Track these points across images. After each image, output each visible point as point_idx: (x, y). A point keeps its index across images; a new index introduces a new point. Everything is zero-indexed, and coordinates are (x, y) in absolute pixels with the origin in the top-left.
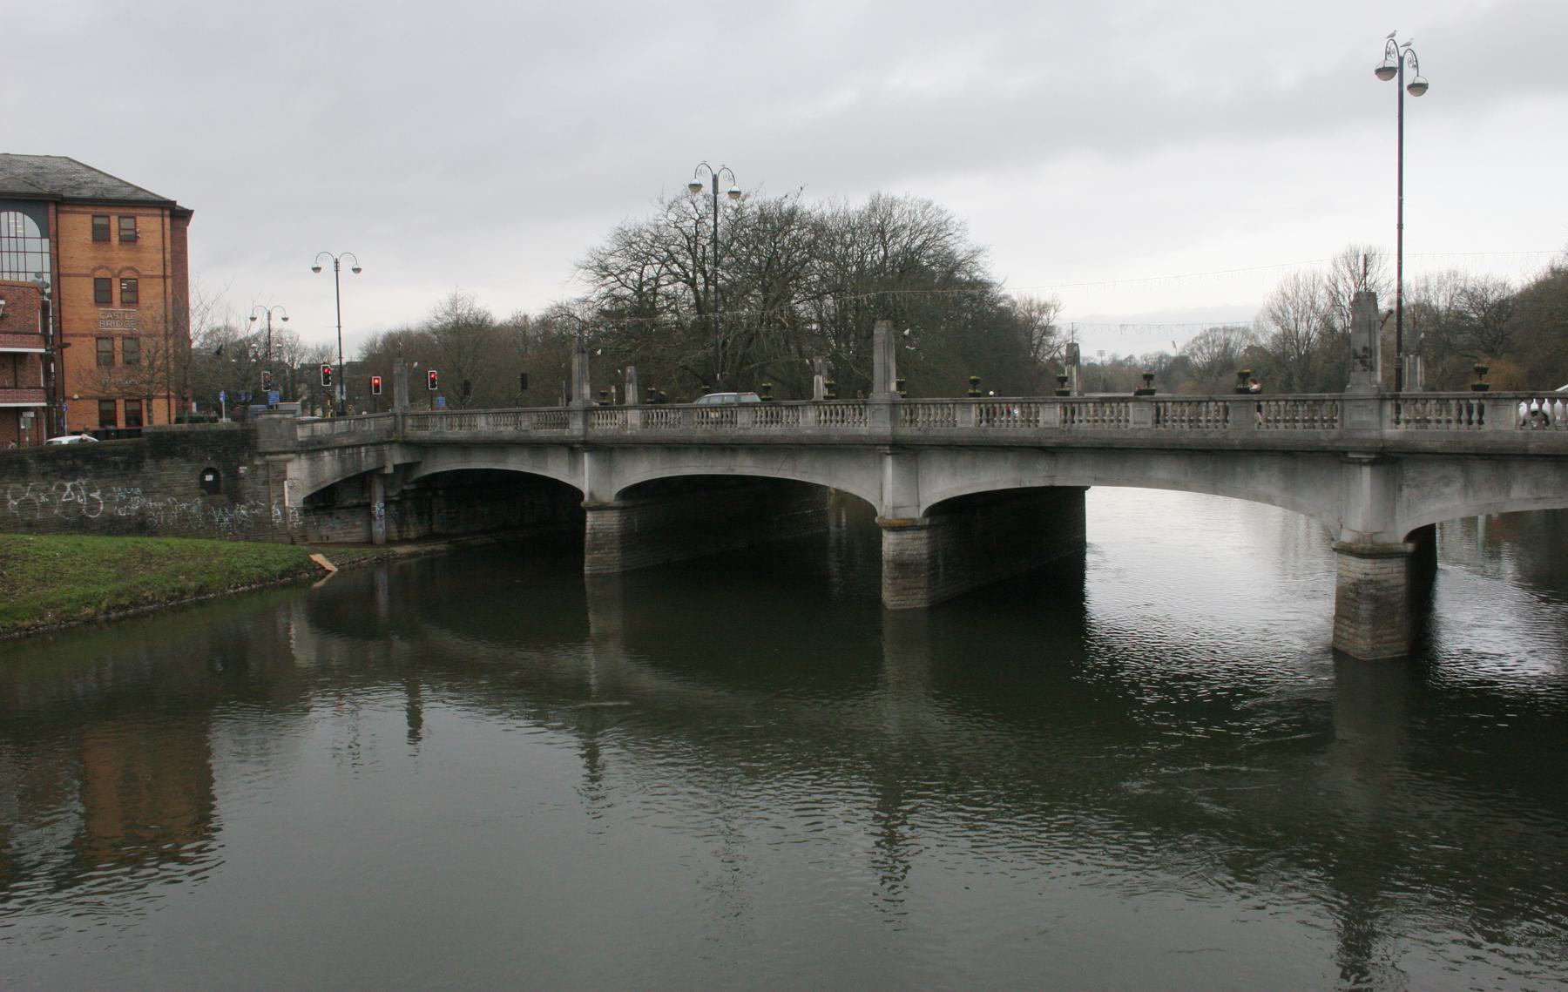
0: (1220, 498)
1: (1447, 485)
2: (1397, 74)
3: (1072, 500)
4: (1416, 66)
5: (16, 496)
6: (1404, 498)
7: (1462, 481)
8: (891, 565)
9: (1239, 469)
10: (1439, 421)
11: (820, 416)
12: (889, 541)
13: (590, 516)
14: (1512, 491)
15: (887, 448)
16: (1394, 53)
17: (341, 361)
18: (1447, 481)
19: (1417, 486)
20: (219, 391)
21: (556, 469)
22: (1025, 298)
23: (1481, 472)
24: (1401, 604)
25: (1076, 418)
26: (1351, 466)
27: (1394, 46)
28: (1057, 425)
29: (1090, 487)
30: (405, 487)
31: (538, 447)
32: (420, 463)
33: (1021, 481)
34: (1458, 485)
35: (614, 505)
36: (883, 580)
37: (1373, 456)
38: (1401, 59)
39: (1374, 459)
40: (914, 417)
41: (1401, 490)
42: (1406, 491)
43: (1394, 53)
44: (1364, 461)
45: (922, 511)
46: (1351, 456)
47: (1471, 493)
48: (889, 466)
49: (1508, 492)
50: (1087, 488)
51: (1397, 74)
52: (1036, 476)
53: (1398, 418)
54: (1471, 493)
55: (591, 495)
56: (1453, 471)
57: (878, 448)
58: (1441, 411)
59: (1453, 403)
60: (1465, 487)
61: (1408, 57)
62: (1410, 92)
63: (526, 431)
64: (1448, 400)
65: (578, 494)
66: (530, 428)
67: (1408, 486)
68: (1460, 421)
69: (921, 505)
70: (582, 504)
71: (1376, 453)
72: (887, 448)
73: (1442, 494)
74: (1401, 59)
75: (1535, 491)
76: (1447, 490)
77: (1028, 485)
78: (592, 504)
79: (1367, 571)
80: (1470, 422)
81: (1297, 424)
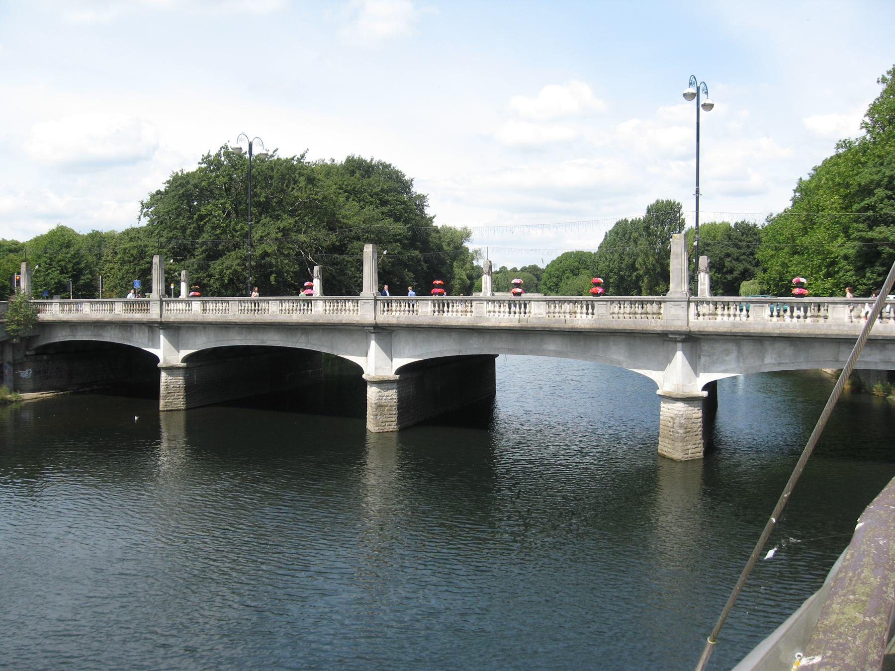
0: (690, 368)
1: (727, 355)
2: (696, 97)
3: (487, 363)
4: (707, 93)
5: (1, 531)
6: (701, 363)
7: (736, 352)
8: (374, 406)
9: (600, 344)
10: (499, 312)
11: (384, 307)
12: (372, 393)
13: (163, 375)
14: (765, 359)
15: (372, 328)
16: (694, 84)
17: (179, 368)
18: (728, 353)
19: (710, 356)
20: (312, 266)
21: (139, 341)
22: (636, 219)
23: (747, 348)
24: (700, 429)
25: (450, 309)
26: (670, 343)
27: (694, 80)
28: (429, 314)
29: (498, 355)
30: (28, 353)
31: (125, 325)
32: (38, 336)
33: (460, 351)
34: (734, 355)
35: (180, 366)
36: (367, 416)
37: (684, 337)
38: (698, 89)
39: (684, 338)
40: (390, 308)
41: (700, 358)
42: (703, 359)
43: (694, 84)
44: (678, 339)
45: (394, 372)
46: (671, 336)
47: (741, 360)
48: (680, 357)
49: (763, 360)
50: (497, 356)
51: (696, 97)
52: (474, 348)
53: (772, 314)
54: (741, 360)
55: (165, 359)
56: (732, 347)
57: (366, 328)
58: (724, 308)
59: (517, 302)
60: (738, 357)
61: (702, 86)
62: (703, 109)
63: (118, 314)
64: (865, 303)
65: (156, 359)
66: (122, 312)
67: (704, 355)
68: (587, 314)
69: (393, 366)
70: (159, 365)
71: (685, 335)
72: (372, 328)
73: (725, 361)
74: (698, 89)
75: (778, 359)
76: (727, 358)
77: (464, 354)
78: (164, 366)
79: (680, 409)
80: (587, 314)
81: (637, 316)
